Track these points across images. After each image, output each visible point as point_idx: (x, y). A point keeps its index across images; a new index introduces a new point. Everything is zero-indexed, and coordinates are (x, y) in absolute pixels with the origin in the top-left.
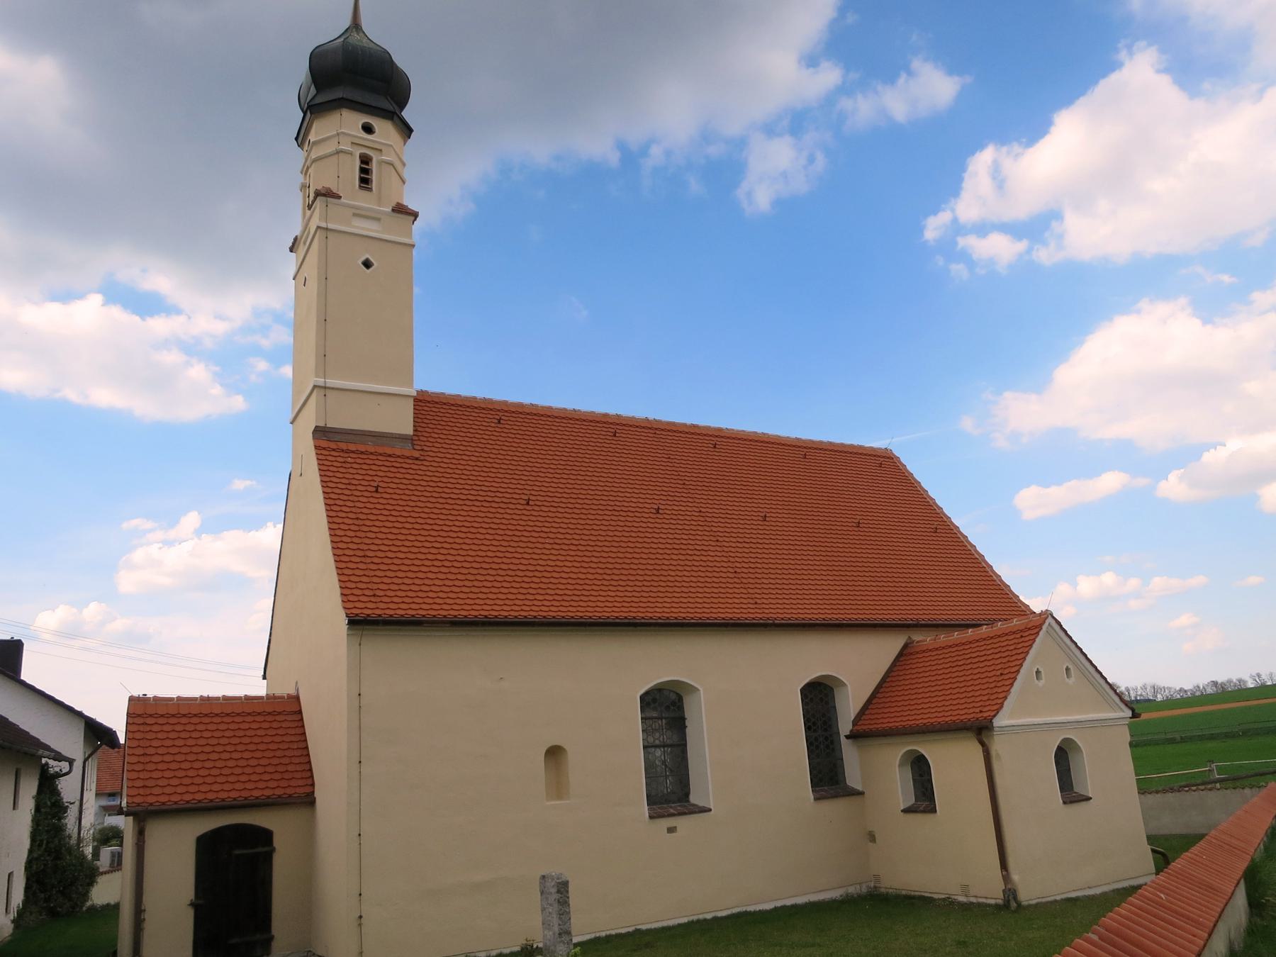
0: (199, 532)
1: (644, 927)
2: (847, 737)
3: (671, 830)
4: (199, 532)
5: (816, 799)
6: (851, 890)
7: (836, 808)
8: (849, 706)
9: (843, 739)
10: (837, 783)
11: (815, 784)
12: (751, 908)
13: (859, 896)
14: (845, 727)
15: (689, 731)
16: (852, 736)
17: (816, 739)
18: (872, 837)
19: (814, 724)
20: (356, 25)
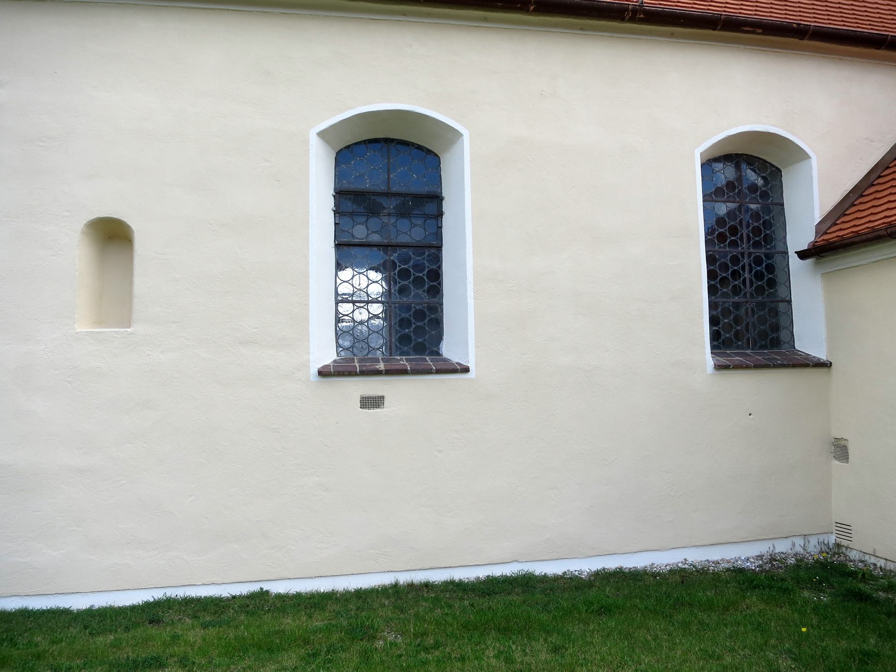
0: (385, 208)
1: (278, 588)
2: (802, 255)
3: (371, 402)
4: (385, 208)
5: (719, 367)
6: (782, 547)
7: (758, 390)
8: (808, 203)
9: (794, 262)
10: (776, 343)
11: (718, 341)
12: (540, 569)
13: (801, 563)
14: (801, 226)
15: (447, 221)
16: (814, 253)
17: (735, 260)
18: (841, 451)
19: (734, 231)
20: (784, 328)
